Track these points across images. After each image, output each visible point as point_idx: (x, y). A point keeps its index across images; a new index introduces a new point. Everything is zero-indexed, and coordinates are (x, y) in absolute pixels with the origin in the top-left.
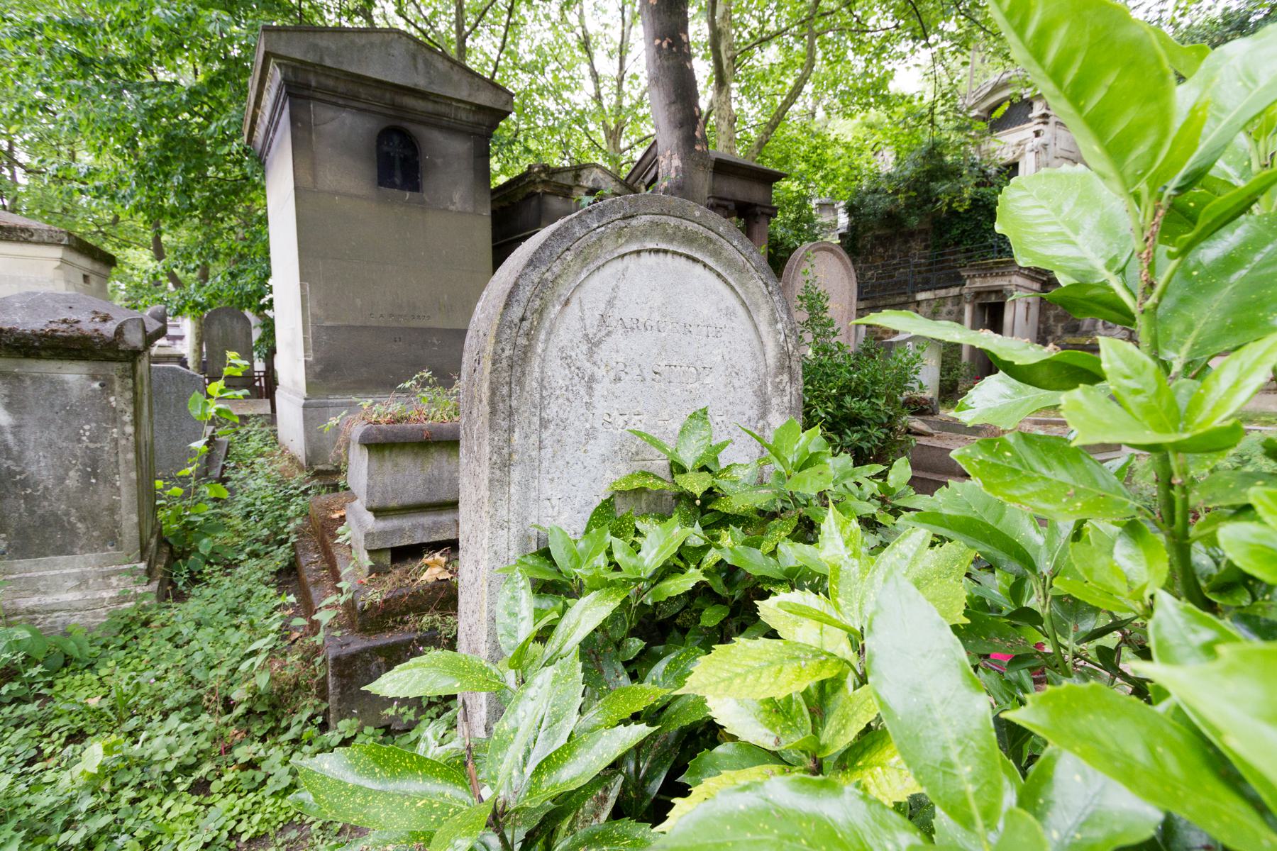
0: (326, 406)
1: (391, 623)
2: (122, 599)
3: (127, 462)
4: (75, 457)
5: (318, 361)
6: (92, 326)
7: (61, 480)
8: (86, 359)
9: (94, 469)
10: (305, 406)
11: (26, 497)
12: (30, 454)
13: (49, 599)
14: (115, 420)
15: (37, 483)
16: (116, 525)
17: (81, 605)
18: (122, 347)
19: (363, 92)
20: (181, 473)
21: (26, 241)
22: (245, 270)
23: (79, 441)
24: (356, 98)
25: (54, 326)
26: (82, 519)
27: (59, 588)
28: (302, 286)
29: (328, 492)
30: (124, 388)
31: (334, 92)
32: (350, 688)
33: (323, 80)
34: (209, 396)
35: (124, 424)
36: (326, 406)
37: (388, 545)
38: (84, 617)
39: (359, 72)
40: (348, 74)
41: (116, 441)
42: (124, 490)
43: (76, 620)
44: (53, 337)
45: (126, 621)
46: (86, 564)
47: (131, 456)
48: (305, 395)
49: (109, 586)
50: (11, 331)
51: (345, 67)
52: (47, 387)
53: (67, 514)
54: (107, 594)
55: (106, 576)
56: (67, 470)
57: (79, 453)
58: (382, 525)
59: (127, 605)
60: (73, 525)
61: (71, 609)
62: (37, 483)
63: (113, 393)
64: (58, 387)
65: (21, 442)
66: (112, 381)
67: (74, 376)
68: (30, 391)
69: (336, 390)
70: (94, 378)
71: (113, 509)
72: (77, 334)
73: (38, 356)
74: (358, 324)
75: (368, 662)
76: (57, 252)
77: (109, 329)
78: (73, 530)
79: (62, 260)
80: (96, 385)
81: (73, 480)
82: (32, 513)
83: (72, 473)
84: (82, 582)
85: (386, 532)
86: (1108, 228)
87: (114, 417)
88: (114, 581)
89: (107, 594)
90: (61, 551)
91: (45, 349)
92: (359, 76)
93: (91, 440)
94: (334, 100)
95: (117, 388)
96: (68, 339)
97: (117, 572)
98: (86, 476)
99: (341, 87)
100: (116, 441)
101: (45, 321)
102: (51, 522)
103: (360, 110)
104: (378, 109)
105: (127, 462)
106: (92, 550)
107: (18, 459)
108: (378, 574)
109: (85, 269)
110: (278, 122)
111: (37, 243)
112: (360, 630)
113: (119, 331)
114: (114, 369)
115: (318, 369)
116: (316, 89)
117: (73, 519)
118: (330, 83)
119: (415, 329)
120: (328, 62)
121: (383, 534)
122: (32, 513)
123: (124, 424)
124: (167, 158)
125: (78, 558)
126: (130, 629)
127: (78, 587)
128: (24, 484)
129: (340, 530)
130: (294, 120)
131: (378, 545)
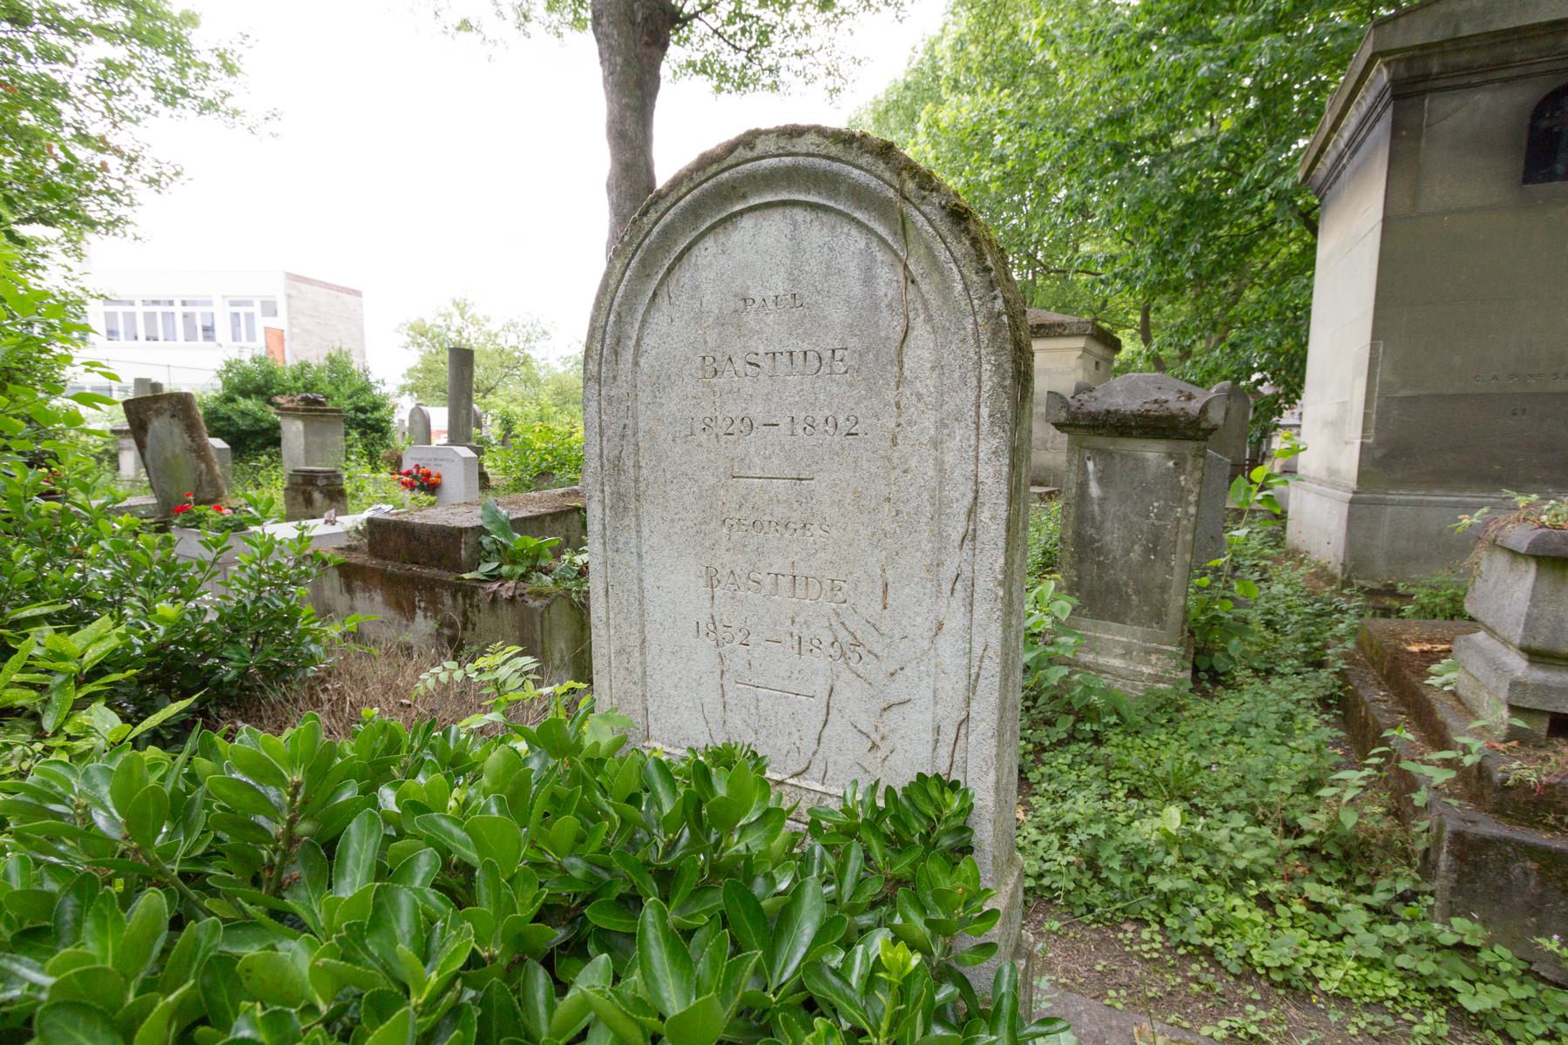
0: (1382, 503)
1: (1550, 819)
2: (1158, 678)
3: (1184, 542)
4: (1142, 532)
5: (1379, 443)
6: (1178, 405)
7: (1127, 552)
8: (1167, 438)
9: (1156, 546)
10: (1352, 502)
11: (1099, 564)
12: (1108, 525)
13: (1101, 660)
14: (1180, 500)
15: (1109, 552)
16: (1164, 604)
17: (1124, 673)
18: (1204, 425)
19: (1518, 51)
20: (1213, 563)
21: (1061, 335)
22: (1249, 339)
23: (1148, 517)
24: (1504, 64)
25: (1147, 407)
26: (1137, 592)
27: (1109, 653)
28: (1373, 347)
29: (1374, 615)
30: (1195, 468)
31: (1469, 70)
32: (1473, 881)
33: (1453, 59)
34: (1251, 482)
35: (1189, 504)
36: (1382, 503)
37: (1550, 708)
38: (1124, 685)
39: (1518, 24)
40: (1495, 34)
41: (1178, 520)
42: (1177, 570)
43: (1117, 686)
44: (1147, 417)
45: (1162, 700)
46: (1134, 636)
47: (1189, 537)
48: (1353, 485)
49: (1148, 663)
50: (1116, 411)
51: (1493, 28)
52: (1131, 464)
53: (1126, 585)
54: (1146, 670)
55: (1148, 652)
56: (1133, 544)
57: (1145, 528)
58: (1539, 675)
59: (1161, 686)
60: (1129, 596)
61: (1116, 674)
62: (1109, 552)
63: (1184, 472)
64: (1140, 463)
65: (1103, 513)
66: (1185, 460)
67: (1153, 454)
68: (1118, 468)
69: (1401, 484)
70: (1170, 456)
71: (1164, 588)
72: (1167, 413)
73: (1130, 435)
74: (1451, 392)
75: (1508, 860)
76: (1080, 343)
77: (1194, 407)
78: (1126, 601)
79: (1084, 350)
80: (1171, 464)
81: (1135, 556)
82: (1100, 578)
83: (1136, 547)
84: (1127, 653)
85: (1549, 688)
86: (597, 744)
87: (1180, 496)
88: (1153, 658)
89: (1146, 670)
90: (1115, 618)
91: (1137, 428)
92: (1516, 30)
93: (1158, 517)
94: (1466, 80)
95: (1189, 467)
96: (1158, 419)
97: (1157, 651)
98: (1147, 551)
99: (1482, 57)
100: (1178, 520)
101: (1140, 402)
102: (1114, 590)
103: (1505, 81)
104: (1546, 67)
105: (1184, 542)
106: (1140, 624)
107: (1099, 529)
108: (1522, 743)
109: (1096, 355)
110: (1363, 140)
111: (1068, 336)
112: (1494, 811)
113: (1204, 410)
114: (1190, 447)
115: (1378, 454)
116: (1438, 76)
117: (1130, 591)
118: (1464, 58)
119: (1557, 395)
120: (1467, 30)
121: (1543, 689)
122: (1100, 578)
123: (1189, 504)
124: (1184, 226)
125: (1128, 628)
126: (1167, 710)
127: (1123, 656)
128: (1099, 551)
129: (1434, 668)
130: (1396, 129)
131: (1530, 702)
